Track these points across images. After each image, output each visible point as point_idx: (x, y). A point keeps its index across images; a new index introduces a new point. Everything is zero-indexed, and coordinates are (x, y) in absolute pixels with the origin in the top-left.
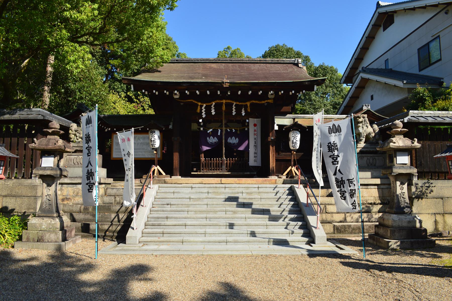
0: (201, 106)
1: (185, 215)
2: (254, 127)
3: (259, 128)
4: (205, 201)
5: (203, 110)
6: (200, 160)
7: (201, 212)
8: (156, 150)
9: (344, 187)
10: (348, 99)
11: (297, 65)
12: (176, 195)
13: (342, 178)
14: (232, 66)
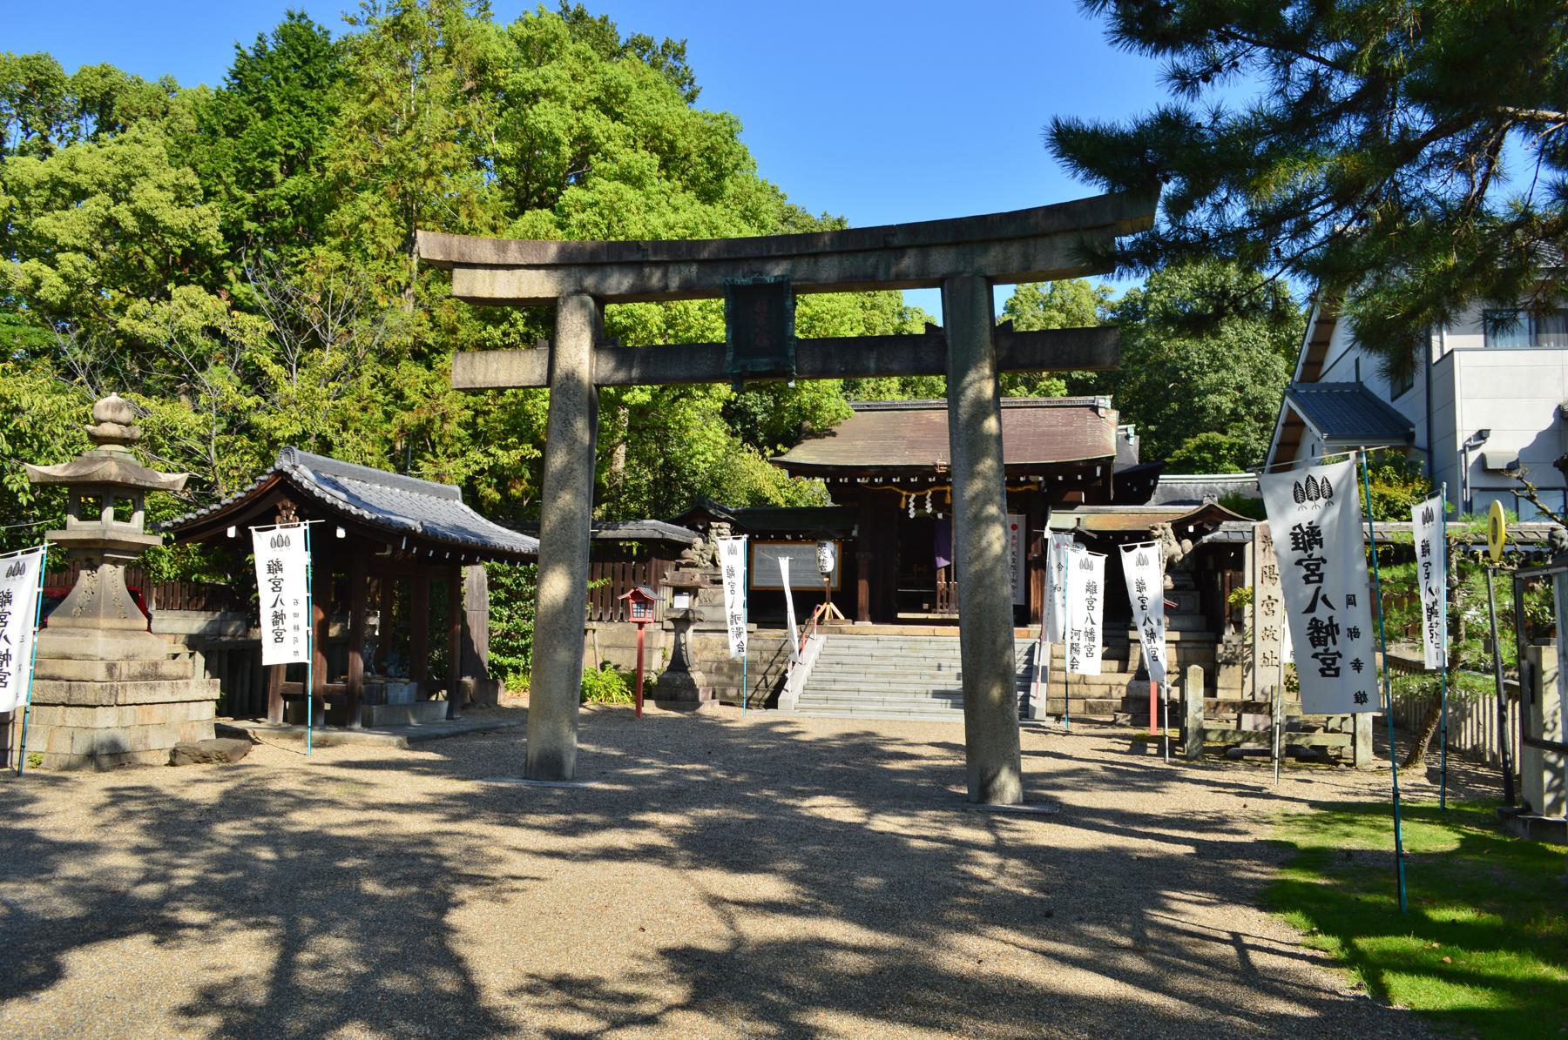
0: (908, 497)
1: (862, 677)
4: (895, 660)
5: (911, 505)
7: (885, 675)
8: (828, 575)
9: (1334, 643)
11: (1095, 409)
12: (852, 651)
13: (1331, 619)
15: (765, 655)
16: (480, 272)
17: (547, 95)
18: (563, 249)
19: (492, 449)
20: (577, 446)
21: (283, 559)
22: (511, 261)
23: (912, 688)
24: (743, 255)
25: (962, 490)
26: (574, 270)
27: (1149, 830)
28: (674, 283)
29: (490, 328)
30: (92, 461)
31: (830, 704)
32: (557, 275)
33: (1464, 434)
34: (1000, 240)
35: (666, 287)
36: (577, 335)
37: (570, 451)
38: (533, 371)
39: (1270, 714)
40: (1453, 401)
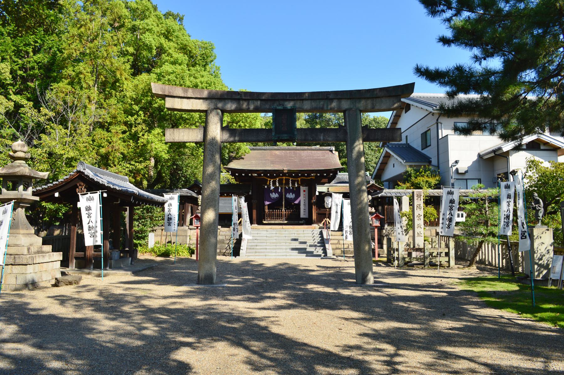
0: (270, 181)
1: (265, 244)
2: (304, 190)
3: (307, 193)
6: (265, 212)
10: (379, 164)
11: (331, 151)
12: (259, 235)
14: (290, 153)
15: (227, 237)
16: (176, 99)
17: (147, 30)
18: (210, 93)
19: (133, 163)
20: (216, 164)
21: (90, 206)
22: (189, 96)
23: (284, 247)
24: (277, 98)
25: (354, 181)
26: (214, 101)
27: (441, 290)
28: (252, 107)
29: (130, 117)
30: (13, 167)
31: (257, 254)
32: (208, 102)
33: (451, 161)
34: (365, 98)
35: (249, 108)
36: (216, 124)
37: (214, 166)
38: (197, 136)
39: (424, 252)
40: (448, 151)
